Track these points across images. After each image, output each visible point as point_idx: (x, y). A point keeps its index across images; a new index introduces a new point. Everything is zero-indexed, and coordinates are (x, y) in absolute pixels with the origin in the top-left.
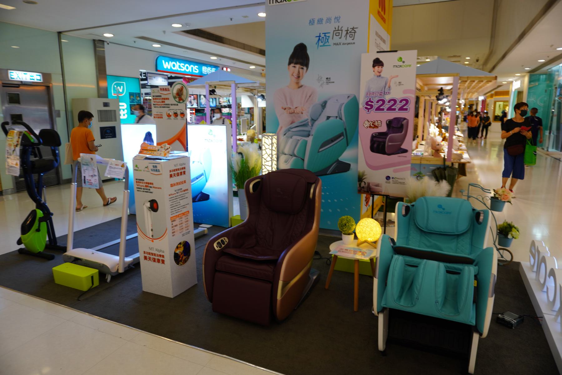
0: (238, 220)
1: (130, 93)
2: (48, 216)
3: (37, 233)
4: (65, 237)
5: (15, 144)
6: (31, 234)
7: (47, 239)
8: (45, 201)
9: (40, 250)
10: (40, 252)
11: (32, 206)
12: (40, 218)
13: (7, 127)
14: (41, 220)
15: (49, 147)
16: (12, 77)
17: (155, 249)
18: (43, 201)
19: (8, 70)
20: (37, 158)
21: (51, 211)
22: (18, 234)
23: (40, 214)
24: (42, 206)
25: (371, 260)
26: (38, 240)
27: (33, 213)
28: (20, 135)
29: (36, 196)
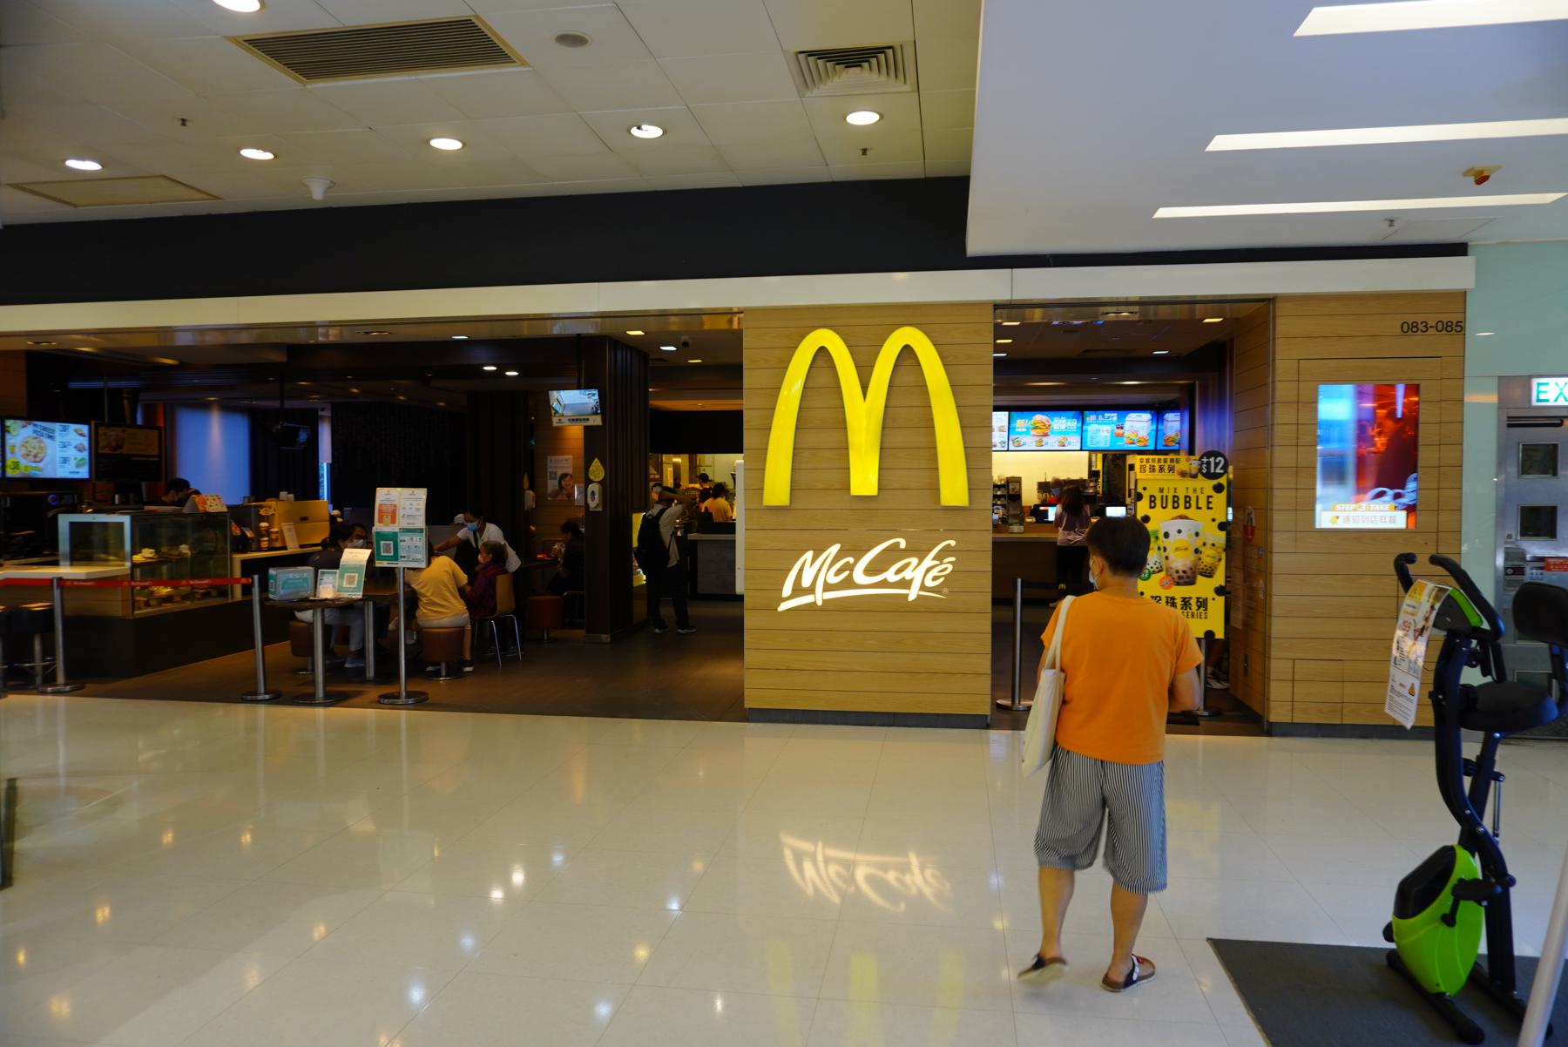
0: (989, 468)
1: (1555, 446)
2: (1494, 891)
3: (1443, 928)
5: (1420, 626)
6: (1423, 926)
7: (1483, 948)
8: (1496, 827)
9: (1443, 988)
10: (1443, 994)
11: (1449, 831)
12: (1461, 881)
13: (1412, 569)
14: (1466, 890)
15: (1545, 646)
18: (1487, 823)
19: (1530, 377)
20: (1489, 679)
21: (1511, 871)
22: (1387, 913)
23: (1469, 866)
24: (1478, 841)
25: (741, 598)
26: (1449, 953)
27: (1442, 861)
28: (1437, 598)
29: (1466, 789)
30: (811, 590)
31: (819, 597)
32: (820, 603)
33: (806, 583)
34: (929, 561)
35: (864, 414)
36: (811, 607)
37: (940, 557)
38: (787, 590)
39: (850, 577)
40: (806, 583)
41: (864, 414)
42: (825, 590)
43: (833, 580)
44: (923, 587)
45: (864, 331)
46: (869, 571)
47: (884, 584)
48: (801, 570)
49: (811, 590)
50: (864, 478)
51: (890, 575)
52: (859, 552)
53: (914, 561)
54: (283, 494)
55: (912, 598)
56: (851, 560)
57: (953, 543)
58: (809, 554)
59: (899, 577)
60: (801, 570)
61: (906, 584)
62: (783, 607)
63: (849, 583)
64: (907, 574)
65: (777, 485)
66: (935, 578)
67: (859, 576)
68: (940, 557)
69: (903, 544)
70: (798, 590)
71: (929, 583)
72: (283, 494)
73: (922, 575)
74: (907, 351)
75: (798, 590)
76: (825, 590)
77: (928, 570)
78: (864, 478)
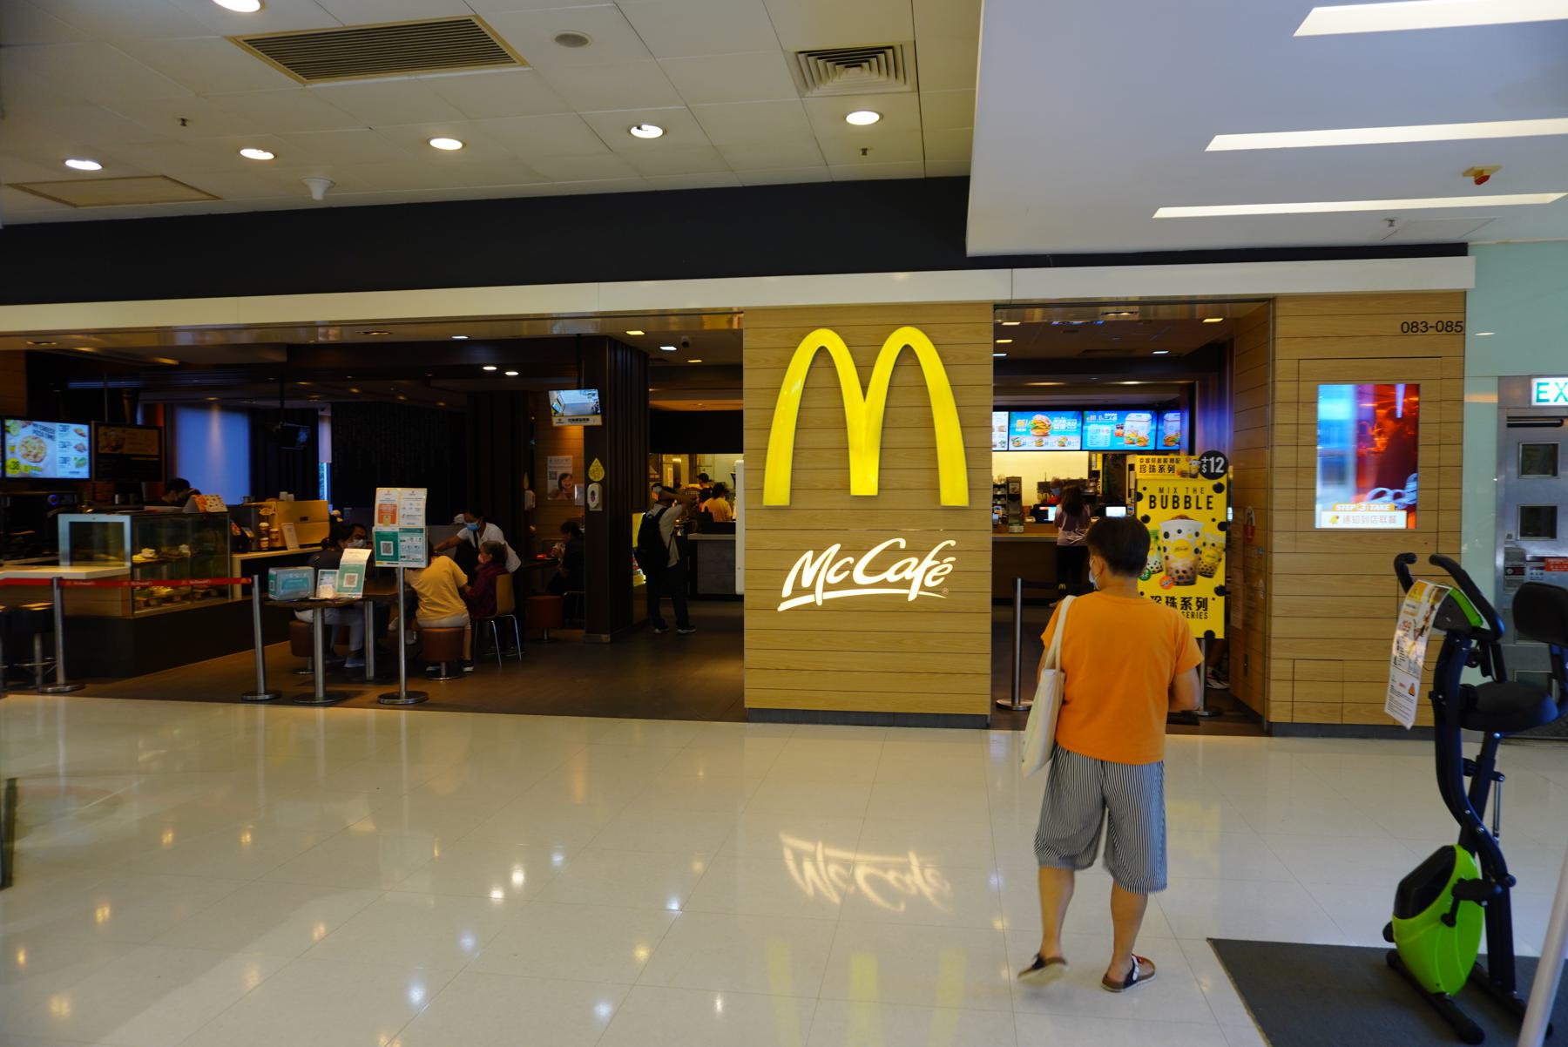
1: (1555, 446)
3: (1443, 928)
4: (1533, 963)
5: (1420, 626)
6: (1423, 926)
7: (1483, 948)
8: (1496, 827)
9: (1443, 988)
10: (1443, 994)
11: (1449, 831)
12: (1461, 881)
13: (1412, 569)
14: (1466, 890)
15: (1545, 646)
16: (1542, 396)
17: (1005, 613)
18: (1487, 823)
19: (1530, 377)
20: (1489, 679)
21: (1511, 871)
22: (1387, 913)
23: (1469, 866)
24: (1478, 841)
26: (1449, 953)
27: (1442, 861)
28: (1437, 598)
30: (811, 590)
31: (819, 597)
32: (820, 603)
33: (806, 583)
34: (929, 561)
35: (864, 414)
36: (811, 607)
37: (940, 557)
38: (787, 590)
39: (850, 577)
40: (806, 583)
41: (864, 414)
42: (825, 590)
43: (833, 580)
44: (923, 587)
45: (864, 331)
46: (869, 571)
47: (884, 584)
48: (801, 570)
49: (811, 590)
50: (864, 478)
51: (890, 575)
52: (859, 552)
53: (914, 561)
54: (283, 494)
55: (912, 598)
56: (851, 560)
57: (953, 543)
58: (809, 554)
59: (899, 577)
60: (801, 570)
61: (906, 584)
62: (783, 607)
63: (849, 583)
64: (907, 574)
65: (777, 485)
66: (935, 578)
67: (859, 576)
68: (940, 557)
69: (903, 544)
70: (798, 590)
71: (929, 583)
72: (283, 494)
73: (922, 575)
74: (907, 351)
75: (798, 590)
76: (825, 590)
77: (928, 570)
78: (864, 478)
